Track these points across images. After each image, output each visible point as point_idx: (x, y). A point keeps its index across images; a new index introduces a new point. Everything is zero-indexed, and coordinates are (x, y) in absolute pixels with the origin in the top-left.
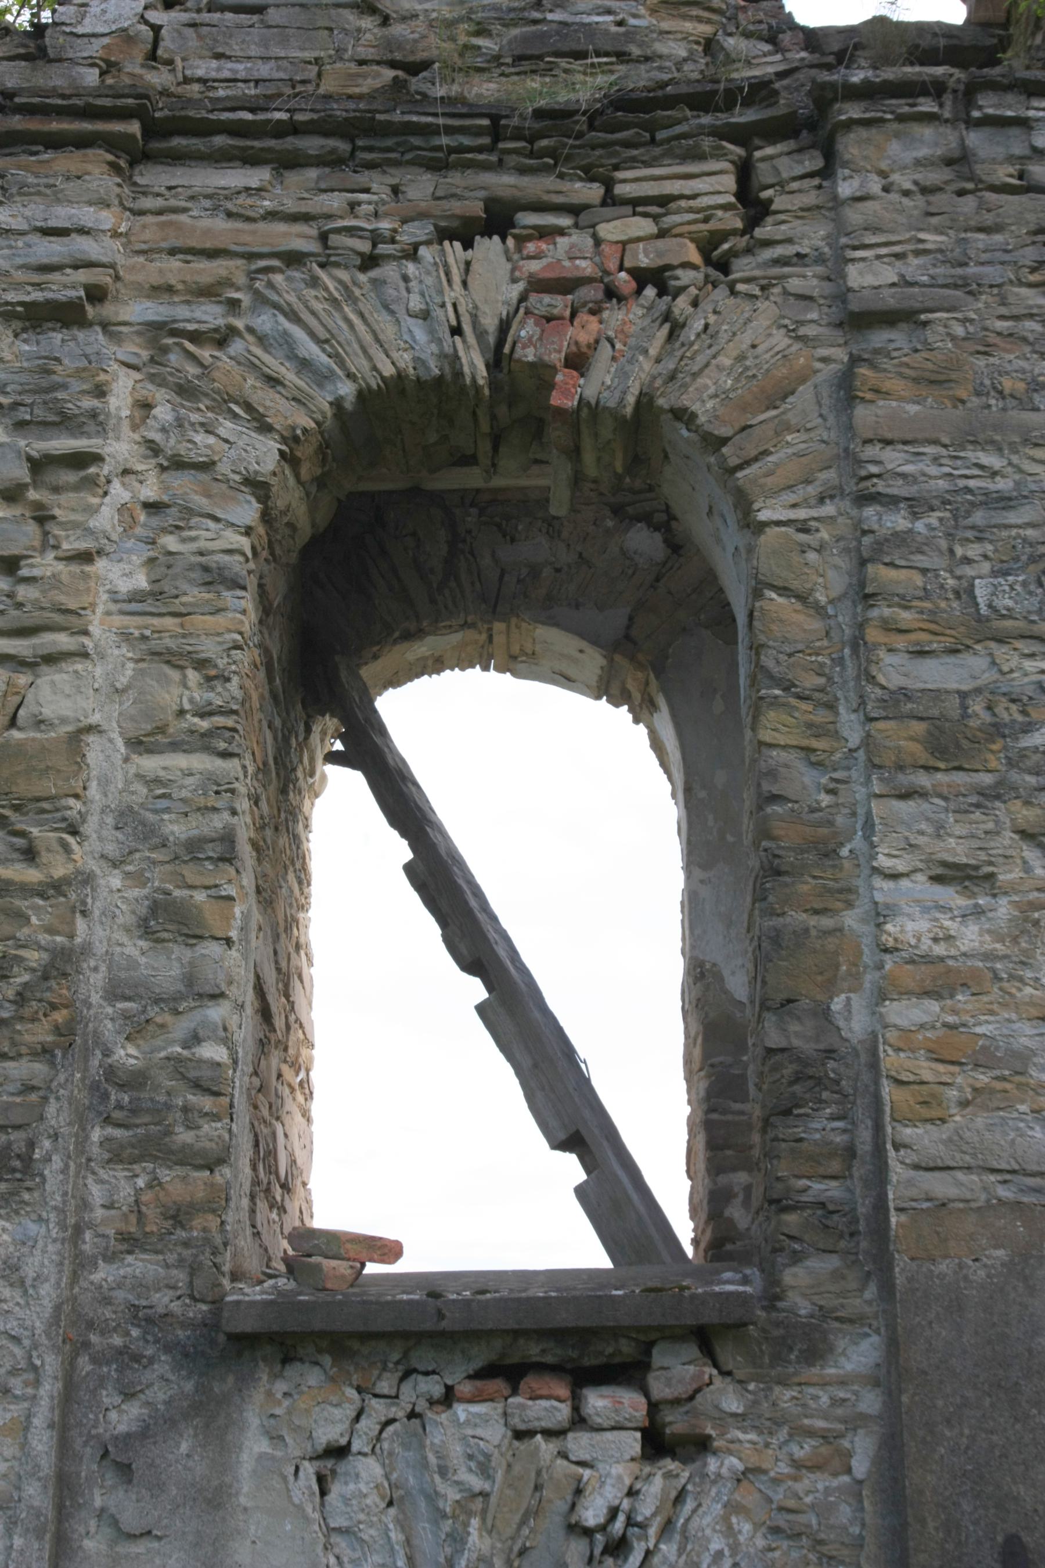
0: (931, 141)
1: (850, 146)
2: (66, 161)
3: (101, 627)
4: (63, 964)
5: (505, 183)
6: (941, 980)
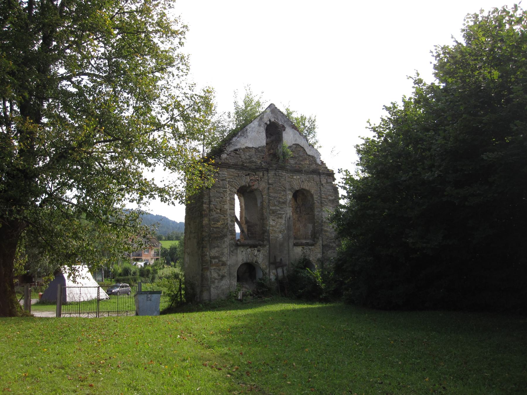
0: (273, 172)
1: (269, 172)
2: (223, 169)
3: (228, 202)
4: (227, 224)
5: (249, 172)
6: (272, 226)
